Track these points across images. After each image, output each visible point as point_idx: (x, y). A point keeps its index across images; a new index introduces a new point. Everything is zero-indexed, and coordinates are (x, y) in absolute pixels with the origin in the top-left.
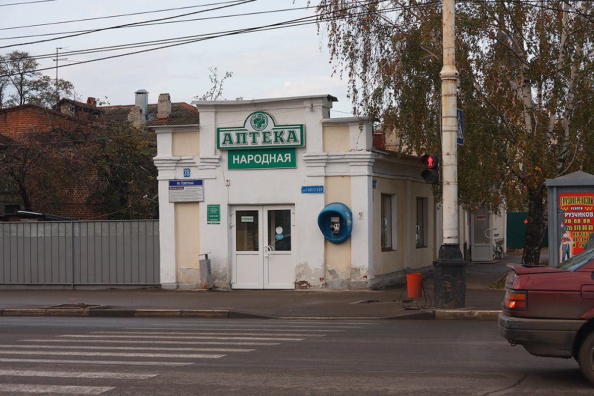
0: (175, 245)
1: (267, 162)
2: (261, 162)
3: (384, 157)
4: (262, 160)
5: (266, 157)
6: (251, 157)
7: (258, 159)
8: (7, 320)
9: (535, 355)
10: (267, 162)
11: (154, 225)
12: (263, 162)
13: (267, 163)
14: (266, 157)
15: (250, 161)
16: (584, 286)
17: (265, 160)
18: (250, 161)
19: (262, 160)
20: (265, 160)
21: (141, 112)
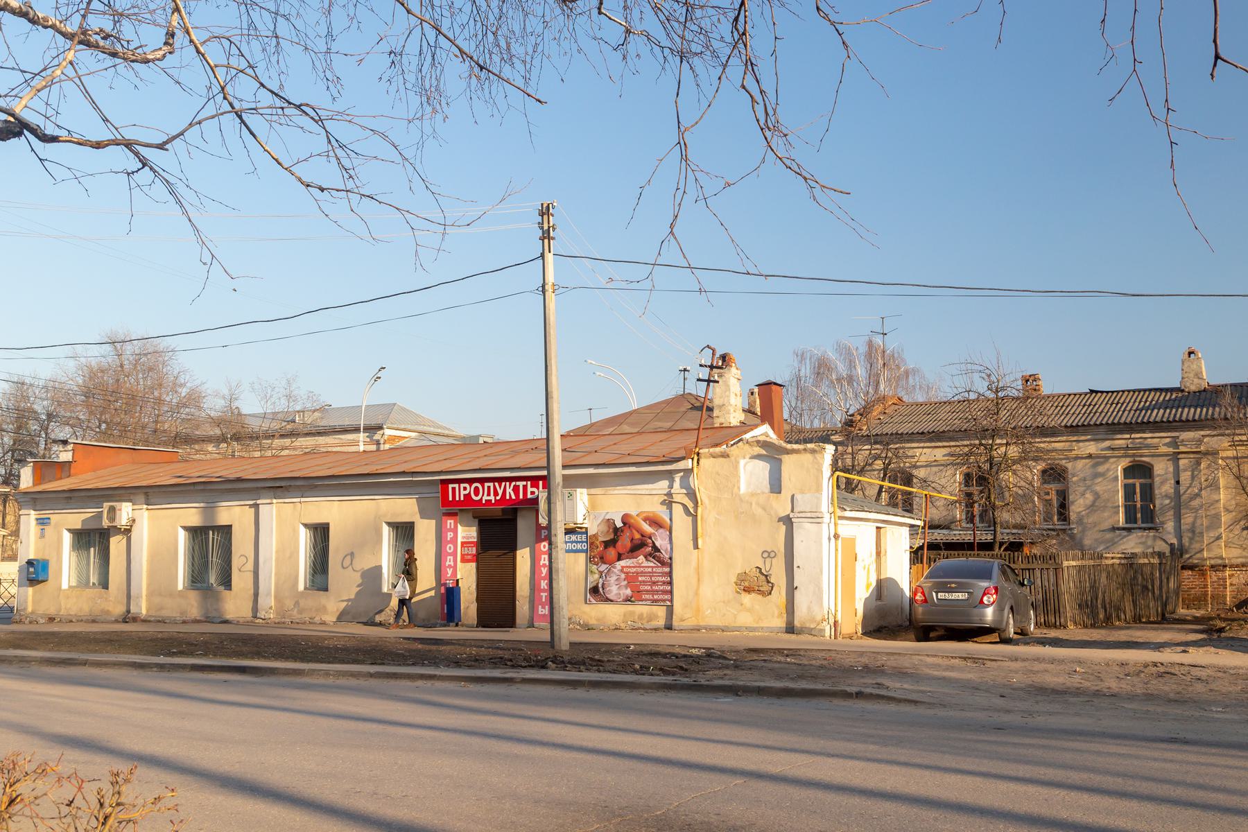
0: (358, 664)
1: (492, 497)
2: (481, 499)
3: (1109, 603)
4: (483, 495)
5: (489, 487)
6: (465, 489)
7: (477, 491)
8: (680, 702)
9: (536, 440)
10: (492, 497)
11: (248, 573)
12: (485, 498)
13: (491, 500)
14: (489, 487)
15: (464, 495)
16: (747, 466)
17: (489, 494)
18: (464, 495)
19: (483, 495)
20: (489, 494)
21: (719, 475)
